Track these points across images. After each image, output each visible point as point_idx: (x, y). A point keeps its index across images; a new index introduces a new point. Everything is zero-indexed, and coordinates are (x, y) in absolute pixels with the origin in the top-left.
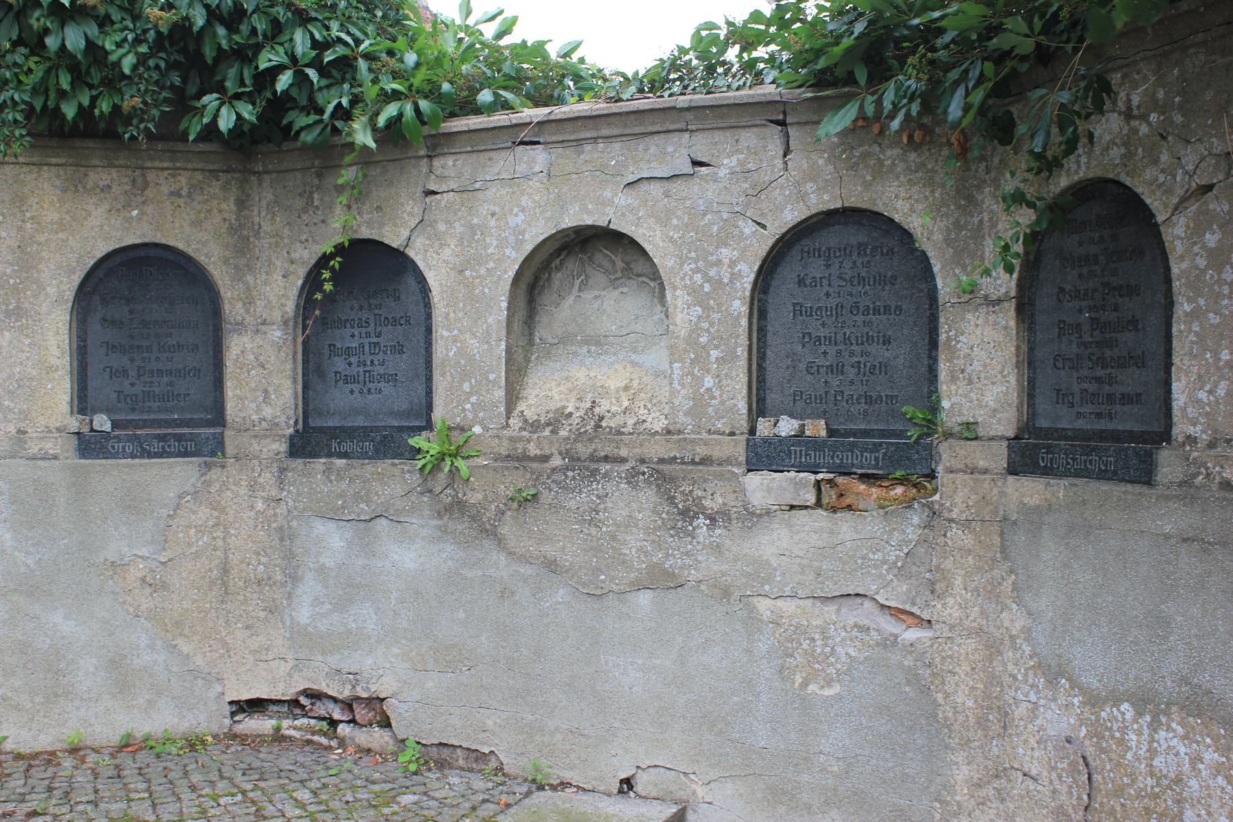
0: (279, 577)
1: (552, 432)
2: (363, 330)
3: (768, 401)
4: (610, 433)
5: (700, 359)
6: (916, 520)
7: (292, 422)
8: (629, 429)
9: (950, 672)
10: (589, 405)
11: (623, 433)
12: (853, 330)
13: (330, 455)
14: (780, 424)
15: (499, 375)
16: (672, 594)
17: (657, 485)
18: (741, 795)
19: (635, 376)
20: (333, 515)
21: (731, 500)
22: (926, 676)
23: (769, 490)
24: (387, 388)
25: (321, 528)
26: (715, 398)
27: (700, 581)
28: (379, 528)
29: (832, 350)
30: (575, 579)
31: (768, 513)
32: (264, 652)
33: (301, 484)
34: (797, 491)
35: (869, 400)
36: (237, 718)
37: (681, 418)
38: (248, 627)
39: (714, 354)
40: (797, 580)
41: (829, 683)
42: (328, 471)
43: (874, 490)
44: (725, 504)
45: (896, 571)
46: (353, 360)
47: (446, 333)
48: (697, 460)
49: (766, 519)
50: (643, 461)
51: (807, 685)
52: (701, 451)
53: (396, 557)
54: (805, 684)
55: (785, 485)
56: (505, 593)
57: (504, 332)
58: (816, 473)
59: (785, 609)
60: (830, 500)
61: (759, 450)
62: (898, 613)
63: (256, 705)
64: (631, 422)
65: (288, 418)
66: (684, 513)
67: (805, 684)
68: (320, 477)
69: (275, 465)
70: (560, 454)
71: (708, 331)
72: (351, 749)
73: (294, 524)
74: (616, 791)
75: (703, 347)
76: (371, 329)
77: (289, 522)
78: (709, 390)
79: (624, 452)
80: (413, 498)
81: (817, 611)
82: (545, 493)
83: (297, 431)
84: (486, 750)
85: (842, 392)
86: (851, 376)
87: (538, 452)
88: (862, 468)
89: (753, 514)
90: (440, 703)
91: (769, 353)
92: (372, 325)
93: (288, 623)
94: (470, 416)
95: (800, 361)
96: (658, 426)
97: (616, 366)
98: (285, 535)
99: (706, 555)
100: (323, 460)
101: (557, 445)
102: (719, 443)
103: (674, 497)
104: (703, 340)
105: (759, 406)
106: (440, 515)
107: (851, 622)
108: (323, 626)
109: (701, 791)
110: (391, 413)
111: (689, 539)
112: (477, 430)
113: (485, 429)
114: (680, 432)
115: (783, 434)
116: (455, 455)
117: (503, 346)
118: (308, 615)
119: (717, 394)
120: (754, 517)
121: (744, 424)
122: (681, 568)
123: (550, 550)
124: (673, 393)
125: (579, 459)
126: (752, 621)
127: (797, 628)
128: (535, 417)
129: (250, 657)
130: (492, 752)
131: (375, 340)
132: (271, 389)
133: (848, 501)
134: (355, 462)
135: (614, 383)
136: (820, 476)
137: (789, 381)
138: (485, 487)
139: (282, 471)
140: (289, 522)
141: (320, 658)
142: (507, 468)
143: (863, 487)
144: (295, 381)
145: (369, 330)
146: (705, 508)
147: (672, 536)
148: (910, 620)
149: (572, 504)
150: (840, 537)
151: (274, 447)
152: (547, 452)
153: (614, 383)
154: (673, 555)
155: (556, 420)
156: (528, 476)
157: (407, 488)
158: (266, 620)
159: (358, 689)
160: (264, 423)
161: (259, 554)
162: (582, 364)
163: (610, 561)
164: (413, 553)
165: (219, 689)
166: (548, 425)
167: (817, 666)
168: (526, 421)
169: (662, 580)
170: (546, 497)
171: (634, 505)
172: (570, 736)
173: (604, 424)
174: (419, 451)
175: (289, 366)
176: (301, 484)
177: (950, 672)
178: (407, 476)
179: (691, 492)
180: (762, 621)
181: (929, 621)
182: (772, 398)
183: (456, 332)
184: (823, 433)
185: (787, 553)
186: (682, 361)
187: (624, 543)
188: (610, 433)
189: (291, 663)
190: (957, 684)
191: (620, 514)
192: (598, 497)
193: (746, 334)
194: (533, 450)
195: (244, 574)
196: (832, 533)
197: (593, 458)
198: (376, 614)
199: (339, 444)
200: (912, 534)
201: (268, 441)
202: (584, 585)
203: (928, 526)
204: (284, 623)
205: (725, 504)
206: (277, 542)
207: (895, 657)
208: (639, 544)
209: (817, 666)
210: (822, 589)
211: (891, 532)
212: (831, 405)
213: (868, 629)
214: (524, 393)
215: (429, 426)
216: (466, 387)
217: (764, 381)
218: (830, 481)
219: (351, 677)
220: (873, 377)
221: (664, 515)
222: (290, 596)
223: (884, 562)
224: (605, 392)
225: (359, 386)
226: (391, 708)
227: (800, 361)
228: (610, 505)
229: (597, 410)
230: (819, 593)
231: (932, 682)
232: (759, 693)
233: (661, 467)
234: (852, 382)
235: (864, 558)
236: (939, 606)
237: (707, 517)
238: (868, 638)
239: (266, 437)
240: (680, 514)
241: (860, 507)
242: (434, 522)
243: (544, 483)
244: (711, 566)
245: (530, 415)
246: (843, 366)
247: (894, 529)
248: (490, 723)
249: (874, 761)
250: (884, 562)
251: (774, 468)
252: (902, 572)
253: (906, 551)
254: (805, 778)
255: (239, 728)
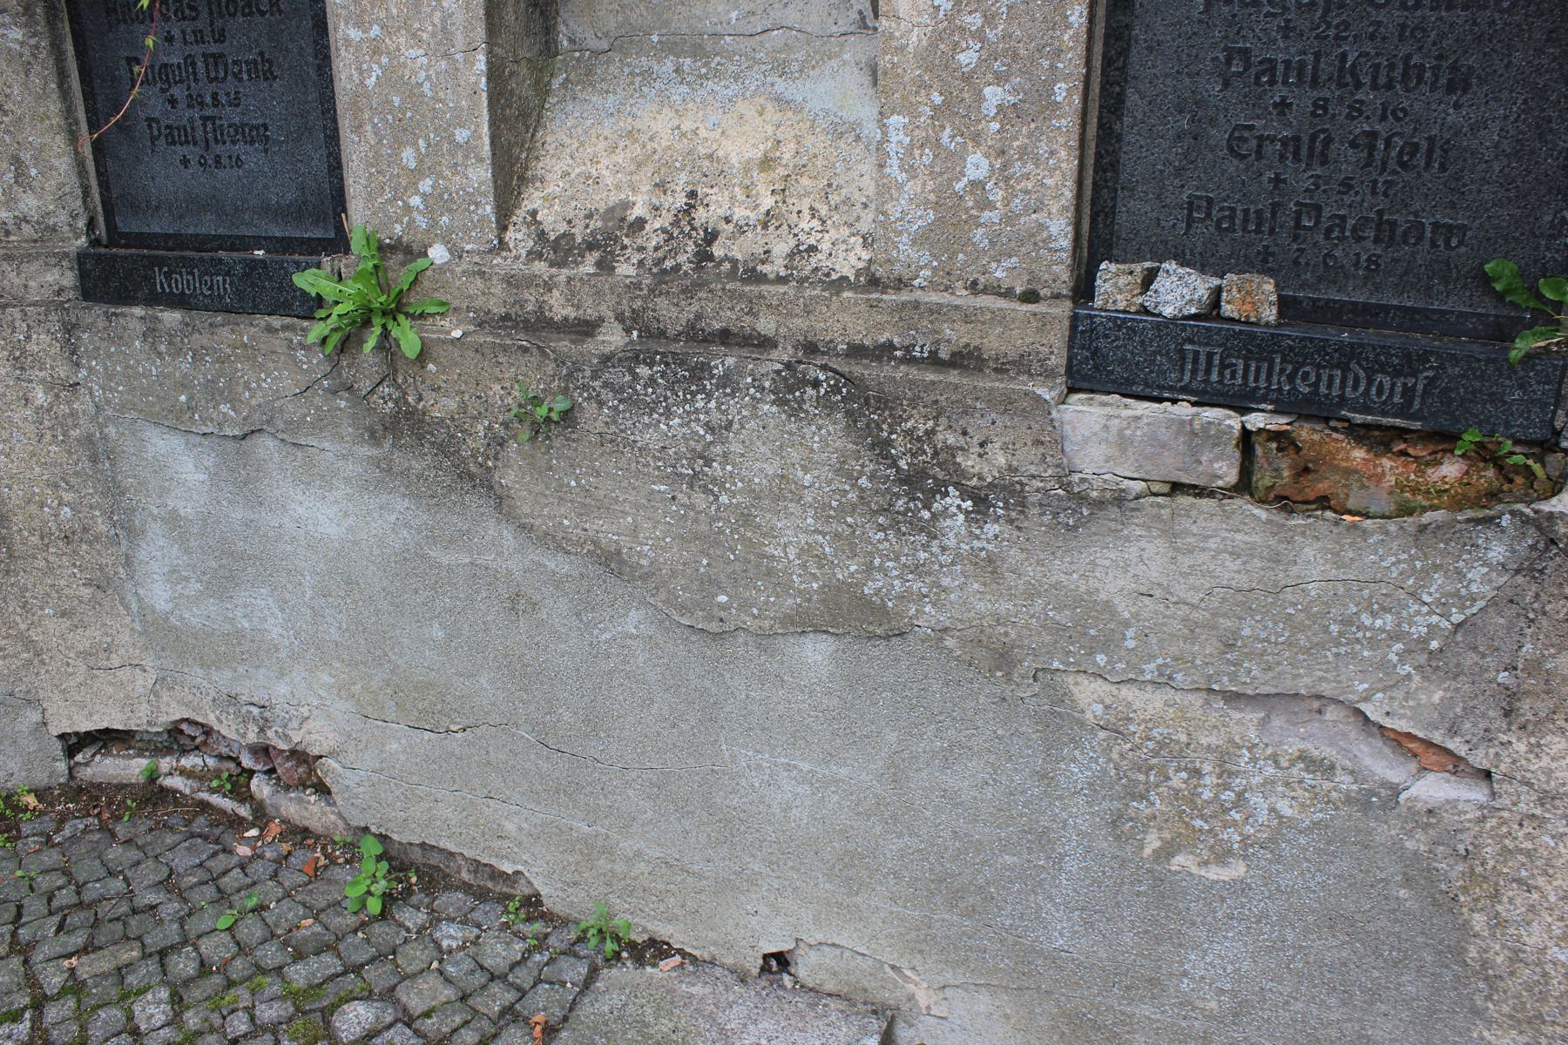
0: (102, 527)
1: (599, 264)
2: (189, 27)
3: (1122, 218)
4: (732, 275)
5: (958, 109)
6: (1497, 552)
7: (81, 224)
8: (775, 267)
9: (1519, 881)
10: (681, 201)
11: (762, 279)
12: (1368, 47)
13: (153, 300)
14: (1161, 283)
15: (477, 131)
16: (878, 650)
17: (849, 413)
18: (1007, 1017)
19: (785, 134)
20: (176, 419)
21: (1028, 460)
22: (1453, 875)
23: (1123, 443)
24: (253, 157)
25: (161, 443)
26: (990, 206)
27: (945, 630)
28: (261, 453)
29: (1303, 100)
30: (663, 595)
31: (1120, 499)
32: (102, 655)
33: (110, 356)
34: (1194, 454)
35: (1386, 232)
36: (79, 758)
37: (906, 252)
38: (64, 614)
39: (994, 95)
40: (1174, 650)
41: (1222, 856)
42: (151, 332)
43: (1387, 463)
44: (1011, 469)
45: (1422, 659)
46: (177, 91)
47: (355, 34)
48: (944, 354)
49: (1113, 512)
50: (811, 348)
51: (1170, 855)
52: (955, 335)
53: (300, 510)
54: (1167, 851)
55: (1164, 435)
56: (518, 604)
57: (480, 32)
58: (1244, 411)
59: (1137, 705)
60: (1279, 482)
61: (1102, 343)
62: (1400, 742)
63: (106, 739)
64: (781, 248)
65: (75, 217)
66: (913, 481)
67: (1167, 851)
68: (139, 346)
69: (53, 317)
70: (620, 318)
71: (979, 35)
72: (275, 828)
73: (111, 431)
74: (755, 971)
75: (967, 78)
76: (202, 23)
77: (101, 427)
78: (977, 185)
79: (766, 325)
80: (318, 401)
81: (1213, 718)
82: (590, 408)
83: (95, 242)
84: (508, 868)
85: (1318, 208)
86: (1346, 170)
87: (570, 312)
88: (1366, 409)
89: (1082, 498)
90: (415, 779)
91: (1132, 98)
92: (205, 15)
93: (134, 606)
94: (422, 222)
95: (1212, 122)
96: (848, 263)
97: (742, 106)
98: (97, 451)
99: (957, 573)
100: (138, 311)
101: (611, 300)
102: (1000, 318)
103: (889, 443)
104: (967, 58)
105: (1098, 239)
106: (374, 438)
107: (1293, 747)
108: (194, 617)
109: (923, 998)
110: (266, 210)
111: (923, 538)
112: (438, 253)
113: (457, 253)
114: (900, 284)
115: (1168, 311)
116: (391, 313)
117: (481, 64)
118: (166, 596)
119: (997, 196)
120: (1083, 507)
121: (1061, 273)
122: (901, 597)
123: (608, 531)
124: (886, 189)
125: (662, 333)
126: (1059, 722)
127: (1161, 745)
128: (563, 228)
129: (80, 662)
130: (517, 873)
131: (214, 49)
132: (26, 156)
133: (1322, 487)
134: (201, 318)
135: (739, 149)
136: (1256, 421)
137: (1179, 172)
138: (474, 388)
139: (70, 329)
140: (101, 427)
141: (200, 672)
142: (505, 348)
143: (1359, 454)
144: (73, 138)
145: (199, 24)
146: (961, 472)
147: (881, 528)
148: (1432, 758)
149: (650, 438)
150: (1294, 570)
151: (50, 278)
152: (591, 314)
153: (739, 149)
154: (881, 568)
155: (610, 236)
156: (550, 368)
157: (304, 381)
158: (94, 603)
159: (270, 734)
160: (26, 228)
161: (56, 486)
162: (664, 99)
163: (738, 567)
164: (330, 506)
165: (35, 717)
166: (591, 246)
167: (1198, 823)
168: (542, 235)
169: (854, 616)
170: (593, 419)
171: (794, 455)
172: (664, 870)
173: (718, 251)
174: (319, 300)
175: (54, 106)
176: (110, 356)
177: (1519, 881)
178: (300, 354)
179: (930, 433)
180: (1082, 724)
181: (1488, 775)
182: (1133, 211)
183: (376, 30)
184: (1270, 314)
185: (1158, 593)
186: (910, 110)
187: (771, 533)
188: (732, 275)
189: (152, 676)
190: (1532, 908)
191: (763, 469)
192: (709, 427)
193: (1081, 49)
194: (559, 307)
195: (36, 524)
196: (1275, 558)
197: (695, 334)
198: (283, 610)
199: (168, 276)
200: (1479, 581)
201: (34, 267)
202: (683, 609)
203: (1529, 570)
204: (127, 608)
205: (1011, 469)
206: (85, 464)
207: (1386, 831)
208: (803, 538)
209: (1198, 823)
210: (1233, 677)
211: (1425, 574)
212: (1284, 237)
213: (1332, 767)
214: (538, 168)
215: (339, 243)
216: (408, 156)
217: (1114, 166)
218: (1276, 436)
219: (255, 711)
220: (1407, 176)
221: (863, 481)
222: (128, 562)
223: (1396, 636)
224: (716, 169)
225: (198, 150)
226: (331, 769)
227: (1212, 122)
228: (736, 448)
229: (700, 215)
230: (1226, 683)
231: (1465, 890)
232: (1062, 857)
233: (856, 369)
234: (1347, 185)
235: (1347, 622)
236: (1522, 747)
237: (966, 494)
238: (1327, 785)
239: (30, 258)
240: (902, 482)
241: (1351, 504)
242: (365, 451)
243: (585, 387)
244: (974, 601)
245: (553, 222)
246: (1328, 141)
247: (1436, 568)
248: (510, 827)
249: (1300, 1006)
250: (1396, 636)
251: (1138, 389)
252: (1436, 664)
253: (1457, 618)
254: (1146, 1010)
255: (86, 774)
